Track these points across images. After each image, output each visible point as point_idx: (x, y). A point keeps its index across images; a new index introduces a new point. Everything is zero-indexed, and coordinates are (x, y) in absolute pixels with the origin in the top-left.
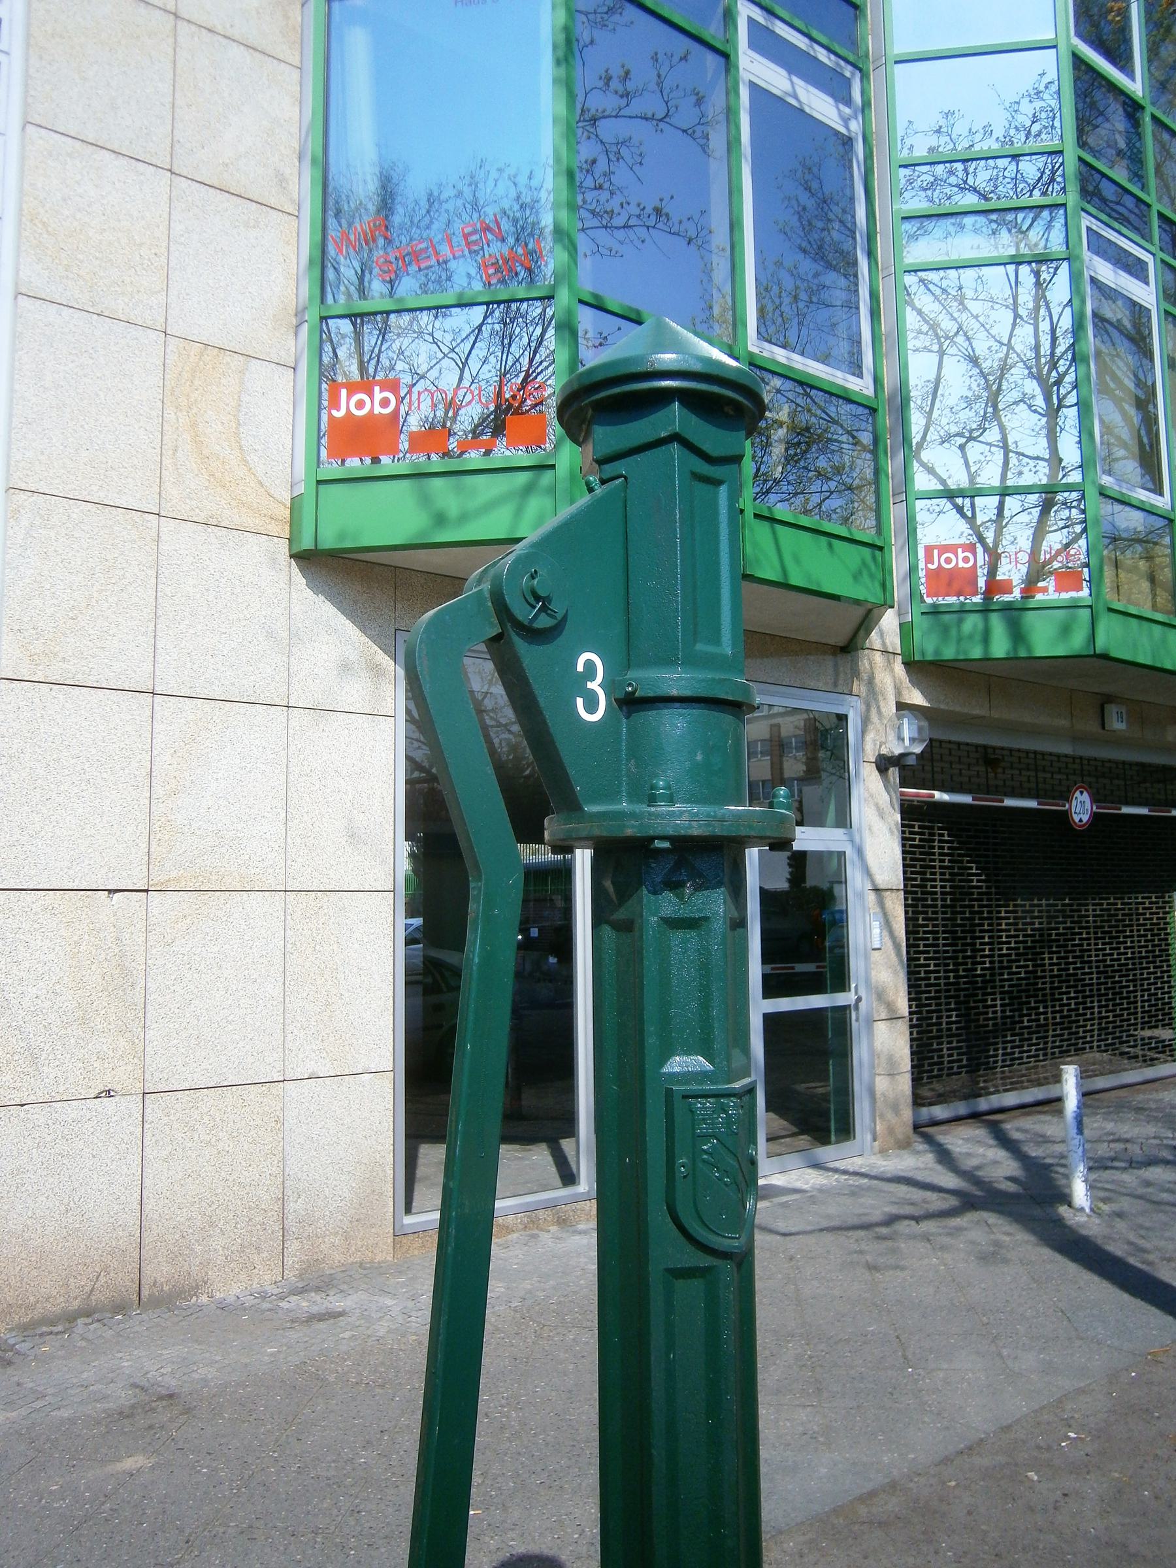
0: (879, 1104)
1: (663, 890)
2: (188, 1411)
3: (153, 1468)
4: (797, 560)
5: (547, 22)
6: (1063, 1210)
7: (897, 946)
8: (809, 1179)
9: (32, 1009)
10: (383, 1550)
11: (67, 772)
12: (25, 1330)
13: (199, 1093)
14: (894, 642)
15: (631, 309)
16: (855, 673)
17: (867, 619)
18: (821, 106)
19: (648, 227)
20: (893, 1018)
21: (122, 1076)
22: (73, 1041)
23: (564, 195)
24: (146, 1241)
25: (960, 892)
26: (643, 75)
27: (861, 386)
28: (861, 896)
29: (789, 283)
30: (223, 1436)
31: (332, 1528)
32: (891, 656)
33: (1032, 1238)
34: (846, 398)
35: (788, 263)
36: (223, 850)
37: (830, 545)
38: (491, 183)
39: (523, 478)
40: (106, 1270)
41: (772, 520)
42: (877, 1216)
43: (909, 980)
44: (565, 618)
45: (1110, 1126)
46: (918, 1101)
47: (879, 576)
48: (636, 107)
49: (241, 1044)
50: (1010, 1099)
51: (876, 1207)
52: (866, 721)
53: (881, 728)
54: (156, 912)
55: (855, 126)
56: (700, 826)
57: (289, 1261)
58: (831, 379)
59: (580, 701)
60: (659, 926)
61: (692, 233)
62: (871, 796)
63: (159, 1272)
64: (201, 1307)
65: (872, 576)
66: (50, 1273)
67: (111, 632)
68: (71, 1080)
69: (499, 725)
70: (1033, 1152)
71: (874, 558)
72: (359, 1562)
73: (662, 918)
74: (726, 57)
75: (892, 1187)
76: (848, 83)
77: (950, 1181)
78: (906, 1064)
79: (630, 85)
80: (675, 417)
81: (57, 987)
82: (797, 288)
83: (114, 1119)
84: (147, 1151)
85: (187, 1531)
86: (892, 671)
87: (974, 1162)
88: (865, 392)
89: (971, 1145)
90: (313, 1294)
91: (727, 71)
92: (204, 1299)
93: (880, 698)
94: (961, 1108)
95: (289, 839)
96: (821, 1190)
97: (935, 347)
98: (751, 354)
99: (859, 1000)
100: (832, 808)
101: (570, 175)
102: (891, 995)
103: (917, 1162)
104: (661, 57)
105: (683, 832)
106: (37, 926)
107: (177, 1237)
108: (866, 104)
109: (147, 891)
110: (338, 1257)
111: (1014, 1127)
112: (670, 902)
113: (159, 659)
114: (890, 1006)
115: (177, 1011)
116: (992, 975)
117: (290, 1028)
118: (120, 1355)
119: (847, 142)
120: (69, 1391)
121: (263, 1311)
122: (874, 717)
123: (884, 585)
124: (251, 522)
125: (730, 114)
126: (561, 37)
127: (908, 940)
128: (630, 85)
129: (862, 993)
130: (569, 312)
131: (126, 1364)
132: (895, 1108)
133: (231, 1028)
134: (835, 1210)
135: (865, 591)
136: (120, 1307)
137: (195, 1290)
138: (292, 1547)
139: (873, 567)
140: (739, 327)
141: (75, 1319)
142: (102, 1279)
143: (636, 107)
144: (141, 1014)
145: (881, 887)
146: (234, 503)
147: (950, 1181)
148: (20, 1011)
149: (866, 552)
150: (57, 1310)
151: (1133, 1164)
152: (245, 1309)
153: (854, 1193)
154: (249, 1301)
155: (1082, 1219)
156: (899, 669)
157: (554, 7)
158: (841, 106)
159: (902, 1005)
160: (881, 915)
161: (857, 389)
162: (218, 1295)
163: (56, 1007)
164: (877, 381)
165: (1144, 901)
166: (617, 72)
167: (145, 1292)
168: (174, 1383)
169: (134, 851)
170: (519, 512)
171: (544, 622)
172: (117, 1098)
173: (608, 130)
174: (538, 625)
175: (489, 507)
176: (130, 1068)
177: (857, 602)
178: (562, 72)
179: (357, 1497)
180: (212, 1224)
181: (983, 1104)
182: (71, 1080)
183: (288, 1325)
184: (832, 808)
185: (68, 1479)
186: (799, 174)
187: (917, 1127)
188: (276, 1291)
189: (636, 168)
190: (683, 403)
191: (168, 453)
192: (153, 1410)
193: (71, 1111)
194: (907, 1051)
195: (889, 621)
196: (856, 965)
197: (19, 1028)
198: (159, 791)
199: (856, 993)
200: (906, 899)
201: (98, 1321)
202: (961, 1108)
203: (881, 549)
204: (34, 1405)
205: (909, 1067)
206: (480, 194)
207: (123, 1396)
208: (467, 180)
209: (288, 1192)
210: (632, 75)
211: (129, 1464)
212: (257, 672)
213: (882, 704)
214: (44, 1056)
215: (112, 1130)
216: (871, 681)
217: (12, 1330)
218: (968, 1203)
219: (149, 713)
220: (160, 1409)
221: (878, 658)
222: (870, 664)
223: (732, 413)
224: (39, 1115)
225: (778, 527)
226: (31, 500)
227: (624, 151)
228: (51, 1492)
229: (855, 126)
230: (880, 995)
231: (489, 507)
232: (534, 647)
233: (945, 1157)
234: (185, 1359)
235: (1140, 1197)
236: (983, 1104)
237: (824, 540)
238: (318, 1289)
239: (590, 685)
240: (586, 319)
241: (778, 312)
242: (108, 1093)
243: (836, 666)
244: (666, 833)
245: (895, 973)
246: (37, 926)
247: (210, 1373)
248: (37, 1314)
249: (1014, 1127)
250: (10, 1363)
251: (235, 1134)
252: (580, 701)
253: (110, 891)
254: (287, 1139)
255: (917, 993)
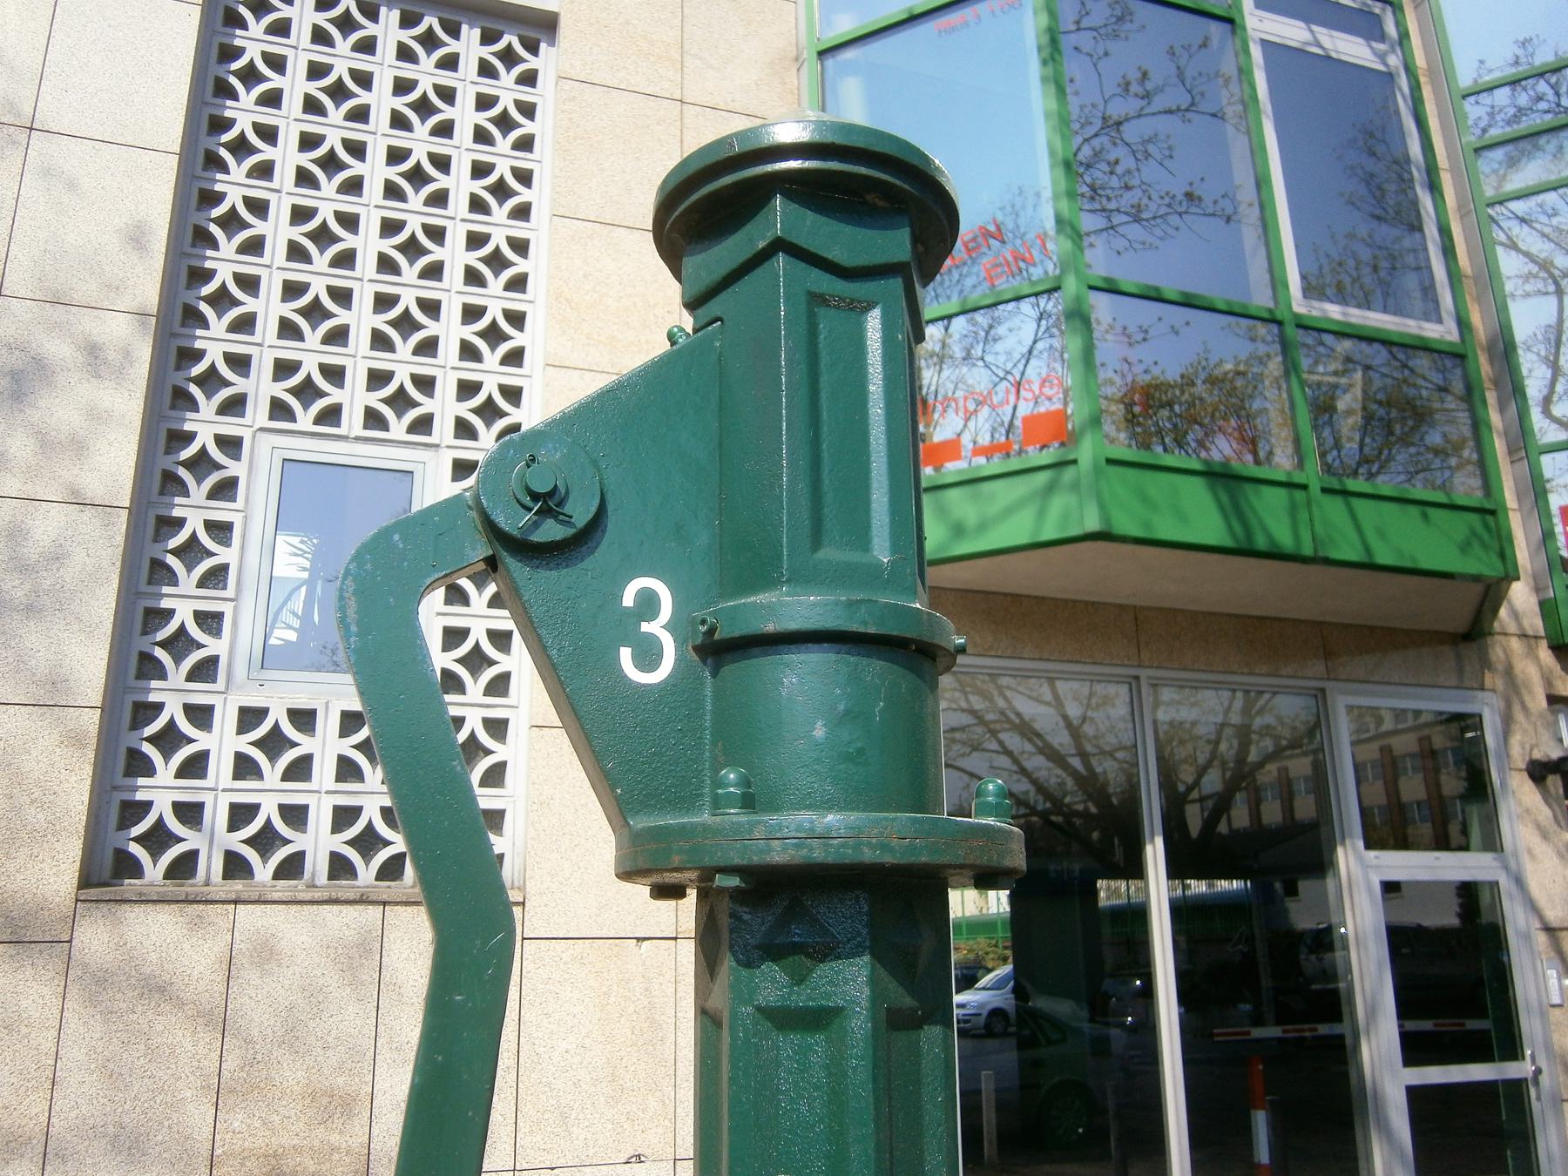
1: (763, 960)
4: (1382, 534)
5: (1030, 26)
14: (1535, 624)
15: (1148, 287)
16: (1485, 663)
17: (1492, 593)
18: (1351, 49)
19: (1180, 214)
23: (1063, 185)
26: (1161, 71)
27: (1442, 331)
28: (1527, 937)
29: (1365, 254)
32: (1532, 641)
34: (1422, 346)
35: (1363, 231)
37: (1425, 516)
38: (1030, 210)
39: (1042, 478)
41: (1345, 493)
44: (597, 523)
47: (1496, 545)
48: (1159, 103)
52: (1507, 721)
53: (1530, 728)
55: (1394, 61)
56: (784, 850)
58: (1402, 329)
59: (626, 654)
60: (755, 1024)
61: (1229, 211)
62: (1527, 811)
65: (1484, 546)
68: (601, 1142)
69: (1103, 752)
71: (1487, 526)
73: (759, 1009)
74: (1230, 22)
76: (1377, 20)
79: (1149, 86)
80: (780, 216)
82: (1375, 257)
86: (1537, 658)
88: (1449, 338)
91: (1233, 32)
93: (1524, 691)
97: (1552, 288)
98: (1297, 316)
99: (1538, 1071)
101: (1067, 165)
104: (1178, 50)
105: (756, 859)
108: (1404, 36)
112: (774, 980)
119: (1390, 76)
122: (1518, 715)
123: (1502, 556)
125: (1244, 73)
126: (1045, 39)
128: (1149, 86)
129: (1543, 1063)
130: (1078, 299)
135: (1481, 564)
139: (1486, 536)
140: (1280, 288)
143: (1159, 103)
145: (1554, 925)
149: (1474, 518)
156: (1545, 655)
157: (1035, 13)
158: (1374, 44)
161: (1435, 335)
164: (1463, 323)
166: (1133, 76)
170: (1041, 514)
171: (551, 531)
172: (647, 1165)
173: (1131, 132)
174: (538, 537)
175: (1009, 511)
177: (1476, 578)
178: (1050, 70)
186: (1361, 143)
189: (1167, 163)
190: (789, 196)
195: (1521, 595)
196: (1529, 1026)
199: (1533, 1062)
203: (1493, 513)
206: (1021, 221)
208: (1009, 209)
210: (1151, 74)
213: (1527, 699)
216: (1509, 672)
221: (1515, 644)
222: (1505, 650)
223: (881, 203)
225: (1356, 502)
227: (1151, 148)
229: (1394, 61)
231: (1009, 511)
232: (543, 574)
237: (1414, 511)
239: (645, 627)
240: (1102, 307)
241: (1357, 286)
242: (639, 1158)
243: (1458, 657)
244: (729, 863)
252: (626, 654)
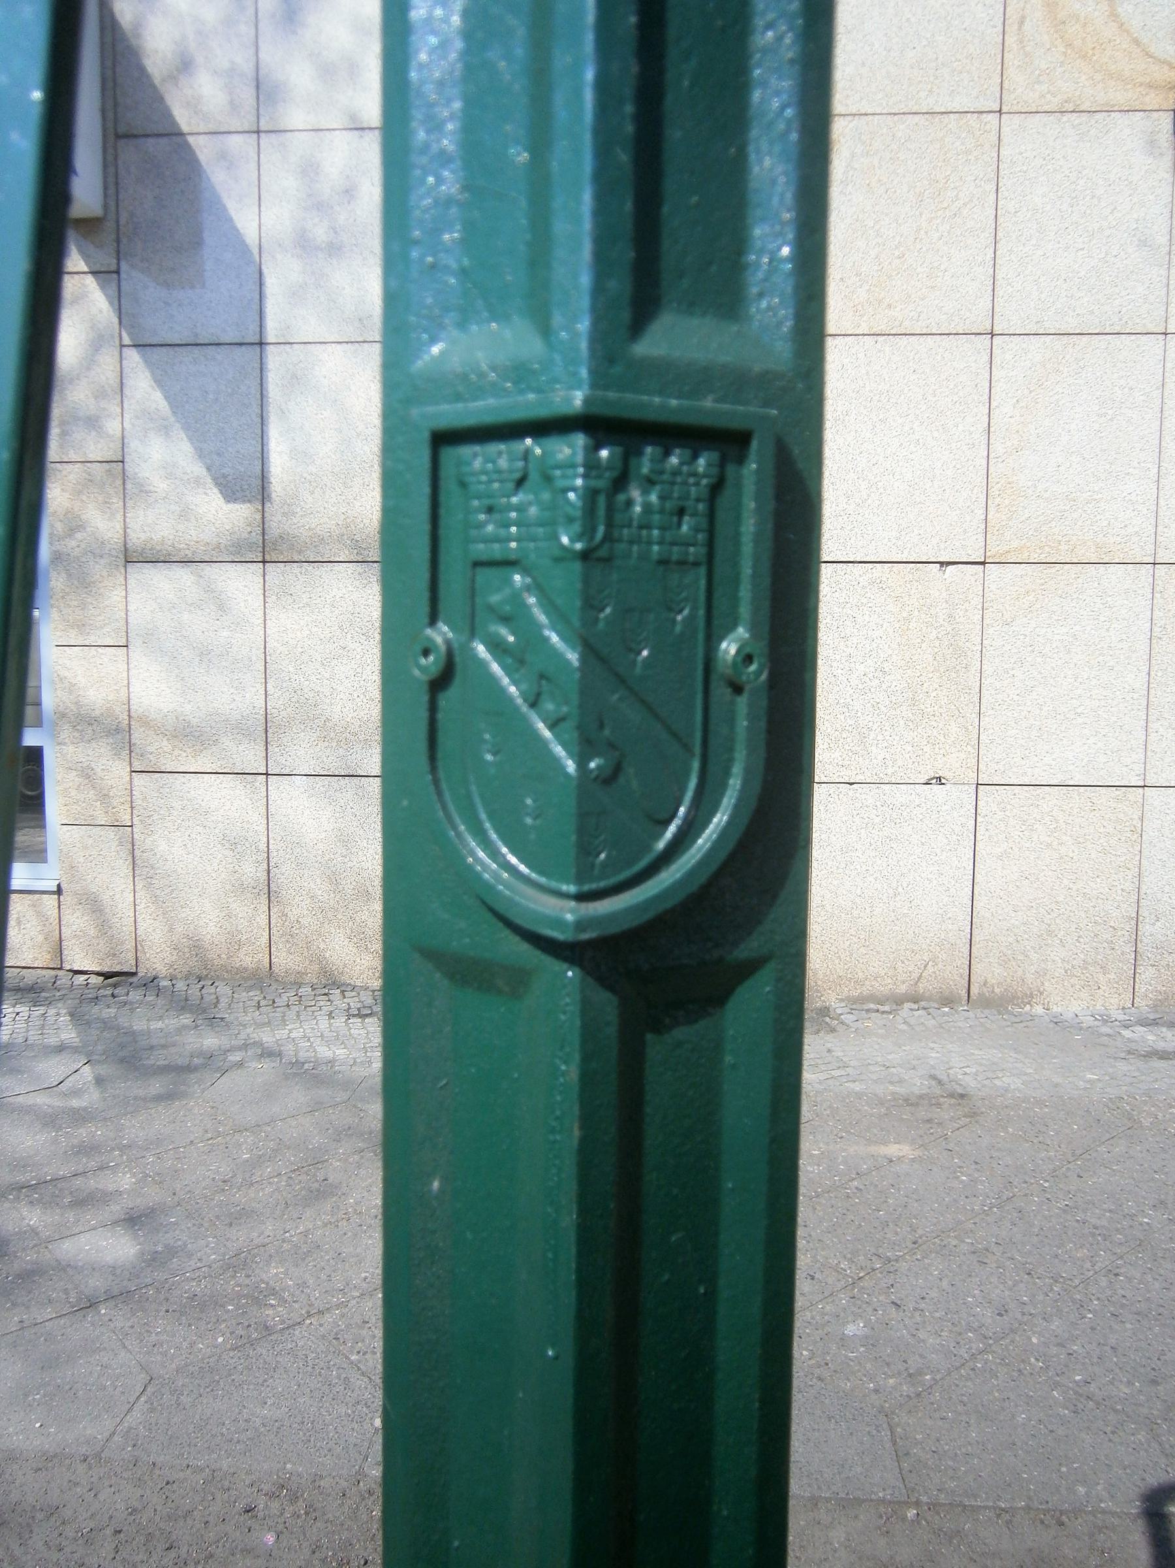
2: (973, 1115)
3: (913, 1160)
9: (860, 686)
10: (1128, 1326)
11: (895, 434)
12: (854, 1003)
13: (1040, 790)
21: (954, 764)
22: (902, 722)
30: (999, 1150)
31: (1077, 1282)
36: (1075, 515)
40: (934, 960)
49: (1092, 740)
54: (993, 587)
57: (1141, 989)
64: (1033, 1018)
66: (878, 952)
67: (942, 267)
68: (900, 763)
72: (1093, 1329)
81: (885, 665)
83: (946, 807)
85: (920, 1232)
90: (1164, 1029)
92: (1039, 1010)
95: (1161, 501)
106: (865, 601)
107: (1010, 939)
109: (983, 563)
113: (999, 292)
115: (1016, 698)
118: (932, 1045)
120: (871, 1067)
121: (1101, 1035)
124: (1120, 97)
131: (933, 1055)
133: (1080, 720)
136: (948, 1001)
137: (1029, 998)
138: (1022, 1285)
141: (903, 1003)
144: (976, 699)
146: (1098, 77)
148: (848, 688)
150: (885, 990)
152: (1081, 1029)
154: (1088, 1021)
162: (1056, 1009)
163: (884, 687)
167: (975, 990)
168: (973, 1084)
169: (968, 518)
172: (948, 786)
176: (963, 755)
179: (1121, 1258)
180: (1050, 933)
182: (900, 763)
183: (1123, 1055)
185: (831, 1147)
188: (1121, 1017)
191: (1012, 29)
192: (938, 1105)
193: (901, 795)
197: (847, 706)
198: (998, 448)
201: (925, 1009)
204: (833, 1073)
207: (917, 1084)
209: (1144, 912)
211: (893, 1150)
212: (1124, 293)
214: (872, 735)
215: (942, 819)
217: (842, 1000)
219: (987, 358)
220: (945, 1106)
224: (867, 795)
226: (851, 125)
228: (812, 1155)
234: (994, 1064)
242: (939, 780)
246: (865, 601)
247: (1016, 1083)
248: (865, 990)
250: (833, 1030)
251: (1081, 840)
253: (942, 564)
254: (1145, 853)
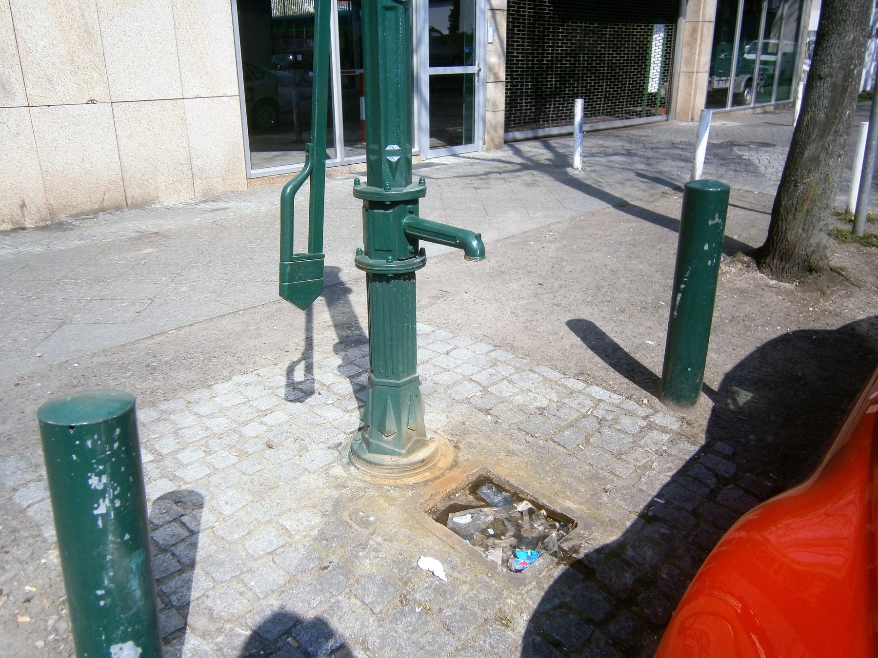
0: (488, 126)
6: (569, 170)
7: (501, 42)
8: (452, 160)
20: (497, 81)
24: (125, 177)
25: (538, 16)
28: (483, 12)
33: (552, 179)
42: (482, 172)
43: (507, 64)
45: (601, 142)
46: (508, 127)
50: (555, 131)
51: (480, 169)
63: (135, 193)
70: (561, 150)
75: (490, 163)
77: (519, 160)
78: (502, 106)
84: (118, 132)
87: (532, 154)
89: (535, 150)
92: (158, 205)
94: (530, 134)
96: (456, 164)
99: (480, 70)
100: (677, 302)
102: (496, 69)
103: (506, 154)
110: (221, 188)
111: (553, 142)
114: (496, 75)
116: (552, 64)
117: (183, 70)
127: (507, 41)
129: (482, 67)
132: (495, 128)
134: (461, 171)
142: (107, 195)
147: (519, 160)
150: (88, 208)
151: (607, 155)
153: (471, 165)
155: (576, 172)
159: (502, 75)
160: (493, 24)
162: (165, 204)
165: (637, 28)
167: (129, 202)
181: (541, 133)
184: (677, 302)
187: (506, 142)
193: (75, 110)
194: (503, 100)
196: (479, 51)
200: (508, 18)
202: (530, 134)
205: (504, 108)
218: (524, 167)
230: (490, 69)
233: (518, 152)
235: (607, 166)
236: (541, 133)
238: (213, 201)
242: (93, 101)
245: (499, 57)
248: (79, 210)
249: (553, 142)
255: (512, 71)
